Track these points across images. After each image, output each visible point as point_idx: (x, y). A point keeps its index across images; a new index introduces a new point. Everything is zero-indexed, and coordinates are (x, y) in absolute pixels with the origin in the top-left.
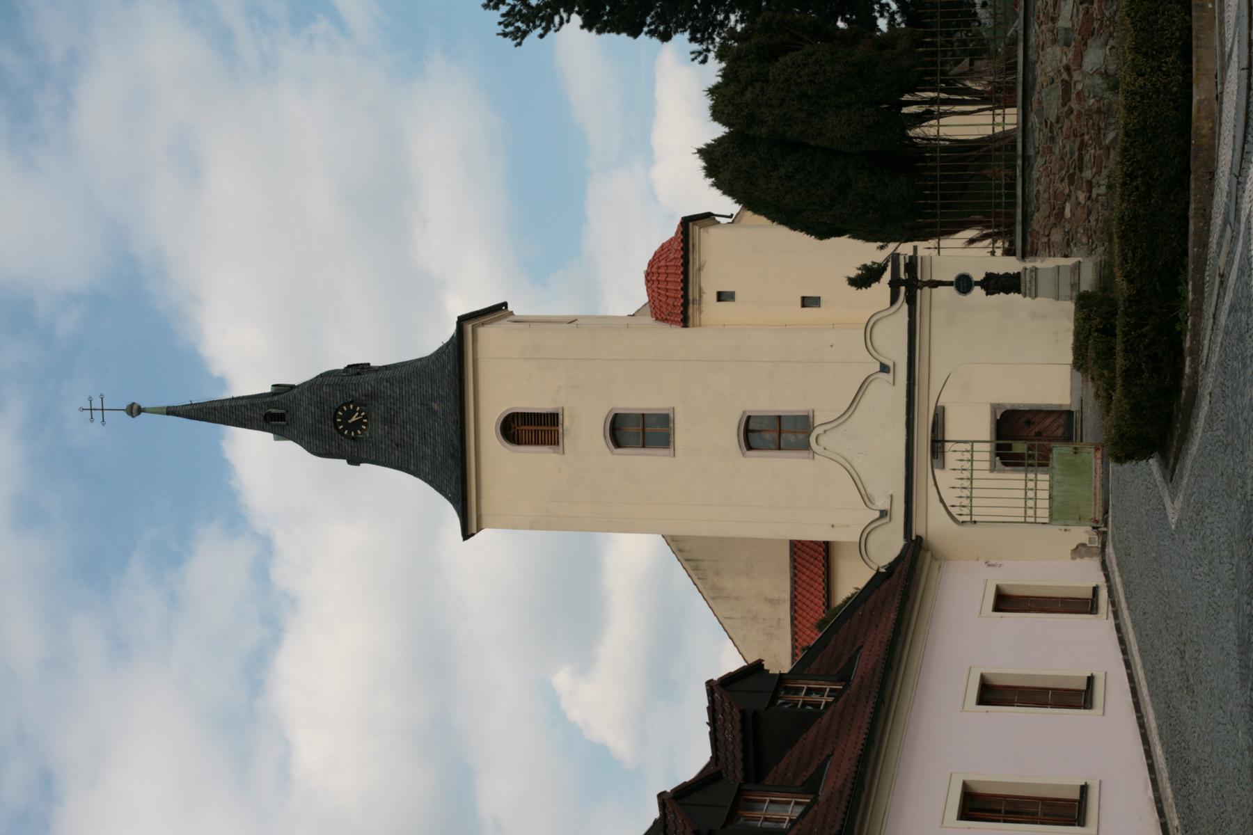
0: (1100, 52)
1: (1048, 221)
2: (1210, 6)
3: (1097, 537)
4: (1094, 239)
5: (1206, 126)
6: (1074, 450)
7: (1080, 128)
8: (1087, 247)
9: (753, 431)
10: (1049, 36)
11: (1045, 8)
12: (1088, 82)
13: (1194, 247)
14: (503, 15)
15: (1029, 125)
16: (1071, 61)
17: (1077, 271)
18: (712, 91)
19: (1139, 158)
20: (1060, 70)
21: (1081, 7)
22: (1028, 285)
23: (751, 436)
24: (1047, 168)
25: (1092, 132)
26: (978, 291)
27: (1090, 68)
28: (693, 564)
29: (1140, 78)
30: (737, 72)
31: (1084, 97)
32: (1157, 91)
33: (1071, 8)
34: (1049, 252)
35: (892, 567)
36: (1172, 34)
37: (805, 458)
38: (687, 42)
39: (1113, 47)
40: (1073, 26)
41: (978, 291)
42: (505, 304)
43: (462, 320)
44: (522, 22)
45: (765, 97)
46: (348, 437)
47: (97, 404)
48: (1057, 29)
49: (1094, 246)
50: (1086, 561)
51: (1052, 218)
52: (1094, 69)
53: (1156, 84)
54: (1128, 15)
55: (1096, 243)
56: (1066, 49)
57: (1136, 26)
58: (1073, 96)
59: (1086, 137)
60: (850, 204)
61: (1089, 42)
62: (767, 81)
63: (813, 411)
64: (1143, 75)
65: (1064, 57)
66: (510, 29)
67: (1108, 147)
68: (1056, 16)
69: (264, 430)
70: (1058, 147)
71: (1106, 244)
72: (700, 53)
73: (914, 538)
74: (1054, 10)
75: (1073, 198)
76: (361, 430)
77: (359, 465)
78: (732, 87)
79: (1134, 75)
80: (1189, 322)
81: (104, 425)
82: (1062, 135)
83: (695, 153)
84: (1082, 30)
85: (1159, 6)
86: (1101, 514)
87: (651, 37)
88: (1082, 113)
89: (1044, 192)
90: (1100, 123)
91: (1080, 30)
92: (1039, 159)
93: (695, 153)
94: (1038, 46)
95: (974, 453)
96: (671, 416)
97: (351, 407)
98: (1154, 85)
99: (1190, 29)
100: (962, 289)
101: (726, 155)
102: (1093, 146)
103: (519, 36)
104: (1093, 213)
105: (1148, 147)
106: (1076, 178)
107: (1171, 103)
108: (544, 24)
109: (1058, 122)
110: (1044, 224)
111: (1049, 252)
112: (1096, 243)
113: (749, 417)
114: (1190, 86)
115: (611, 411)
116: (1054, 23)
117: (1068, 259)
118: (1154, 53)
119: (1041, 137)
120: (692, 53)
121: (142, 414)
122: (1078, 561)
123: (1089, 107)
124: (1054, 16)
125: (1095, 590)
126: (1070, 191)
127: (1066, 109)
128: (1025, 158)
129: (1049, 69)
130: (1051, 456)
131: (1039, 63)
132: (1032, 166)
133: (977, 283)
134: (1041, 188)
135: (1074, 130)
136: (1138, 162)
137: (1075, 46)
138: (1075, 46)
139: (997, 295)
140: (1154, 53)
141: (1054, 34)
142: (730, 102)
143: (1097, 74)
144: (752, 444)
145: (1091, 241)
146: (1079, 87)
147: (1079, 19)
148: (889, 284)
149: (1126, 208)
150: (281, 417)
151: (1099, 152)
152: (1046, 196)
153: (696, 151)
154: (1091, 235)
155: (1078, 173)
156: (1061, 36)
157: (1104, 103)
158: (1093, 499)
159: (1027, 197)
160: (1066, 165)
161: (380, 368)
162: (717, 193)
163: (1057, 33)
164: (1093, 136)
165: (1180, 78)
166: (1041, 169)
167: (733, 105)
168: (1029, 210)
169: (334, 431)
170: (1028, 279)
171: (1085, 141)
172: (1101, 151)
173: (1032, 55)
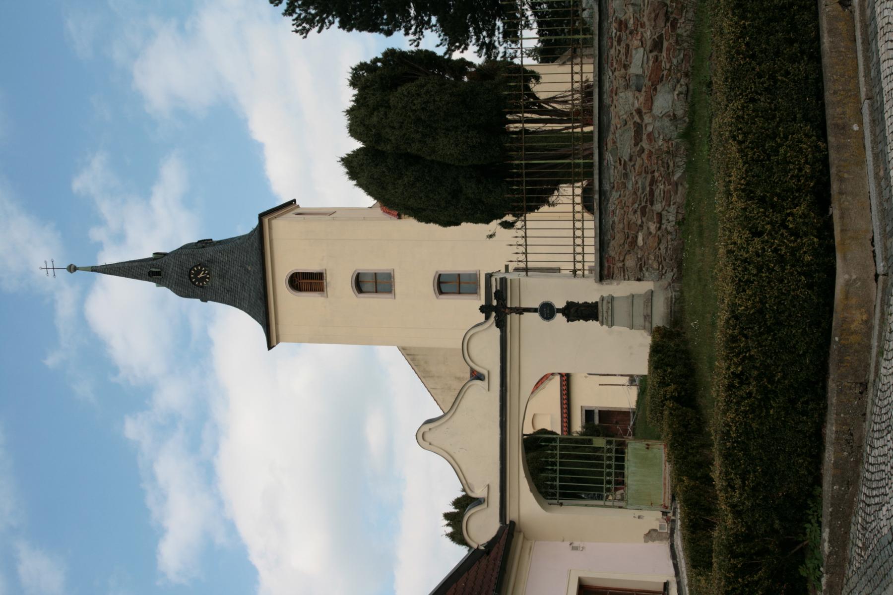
0: (669, 97)
1: (623, 248)
2: (856, 127)
3: (666, 524)
4: (664, 265)
5: (858, 317)
6: (647, 446)
7: (651, 166)
8: (658, 272)
9: (443, 283)
10: (622, 82)
11: (618, 56)
12: (657, 124)
13: (833, 484)
14: (294, 20)
15: (605, 163)
16: (642, 105)
17: (650, 304)
18: (350, 112)
19: (752, 353)
20: (632, 113)
21: (651, 55)
22: (605, 315)
23: (442, 286)
24: (621, 201)
25: (662, 169)
26: (559, 317)
27: (660, 111)
28: (411, 357)
29: (756, 239)
30: (365, 98)
31: (655, 138)
32: (781, 260)
33: (642, 56)
34: (624, 276)
35: (490, 545)
36: (800, 170)
37: (474, 299)
38: (403, 36)
39: (680, 93)
40: (644, 72)
41: (559, 317)
42: (294, 200)
43: (261, 216)
44: (307, 23)
45: (388, 121)
46: (198, 286)
47: (50, 265)
48: (629, 75)
49: (664, 271)
50: (657, 544)
51: (626, 246)
52: (663, 113)
53: (781, 250)
54: (734, 138)
55: (666, 268)
56: (637, 94)
57: (746, 155)
58: (645, 137)
59: (656, 174)
60: (462, 207)
61: (659, 87)
62: (390, 107)
63: (479, 271)
64: (759, 234)
65: (636, 101)
66: (300, 28)
67: (676, 183)
68: (629, 63)
69: (149, 280)
70: (631, 183)
71: (675, 270)
72: (415, 41)
73: (508, 522)
74: (626, 58)
75: (645, 228)
76: (206, 281)
77: (206, 302)
78: (363, 110)
79: (747, 234)
80: (824, 581)
81: (55, 277)
82: (635, 172)
83: (340, 161)
84: (652, 76)
85: (778, 126)
86: (670, 501)
87: (380, 33)
88: (652, 152)
89: (619, 223)
90: (669, 161)
91: (650, 76)
92: (614, 193)
93: (340, 161)
94: (612, 91)
95: (585, 247)
96: (392, 274)
97: (199, 268)
98: (776, 251)
99: (825, 162)
100: (545, 316)
101: (362, 165)
102: (662, 182)
103: (305, 32)
104: (662, 241)
105: (766, 339)
106: (647, 210)
107: (803, 278)
108: (319, 25)
109: (630, 160)
110: (619, 251)
111: (624, 276)
112: (666, 268)
113: (440, 275)
114: (831, 250)
115: (355, 271)
116: (626, 70)
117: (641, 282)
118: (775, 199)
119: (616, 174)
120: (410, 41)
121: (77, 271)
122: (650, 544)
123: (659, 147)
124: (626, 63)
125: (666, 585)
126: (642, 222)
127: (638, 149)
128: (602, 192)
129: (622, 112)
130: (626, 451)
131: (613, 107)
132: (608, 200)
133: (559, 311)
134: (616, 219)
135: (645, 168)
136: (751, 358)
137: (646, 91)
138: (646, 91)
139: (577, 322)
140: (775, 199)
141: (626, 80)
142: (361, 123)
143: (666, 117)
144: (443, 290)
145: (661, 266)
146: (650, 129)
147: (649, 66)
148: (480, 309)
149: (733, 420)
150: (158, 274)
151: (668, 187)
152: (621, 226)
153: (340, 160)
154: (662, 261)
155: (649, 206)
156: (633, 81)
157: (672, 144)
158: (663, 489)
159: (603, 228)
160: (639, 199)
161: (220, 242)
162: (361, 192)
163: (629, 79)
164: (663, 173)
165: (815, 240)
166: (616, 202)
167: (364, 125)
168: (606, 238)
169: (190, 282)
170: (605, 310)
171: (656, 177)
172: (670, 187)
173: (607, 100)
